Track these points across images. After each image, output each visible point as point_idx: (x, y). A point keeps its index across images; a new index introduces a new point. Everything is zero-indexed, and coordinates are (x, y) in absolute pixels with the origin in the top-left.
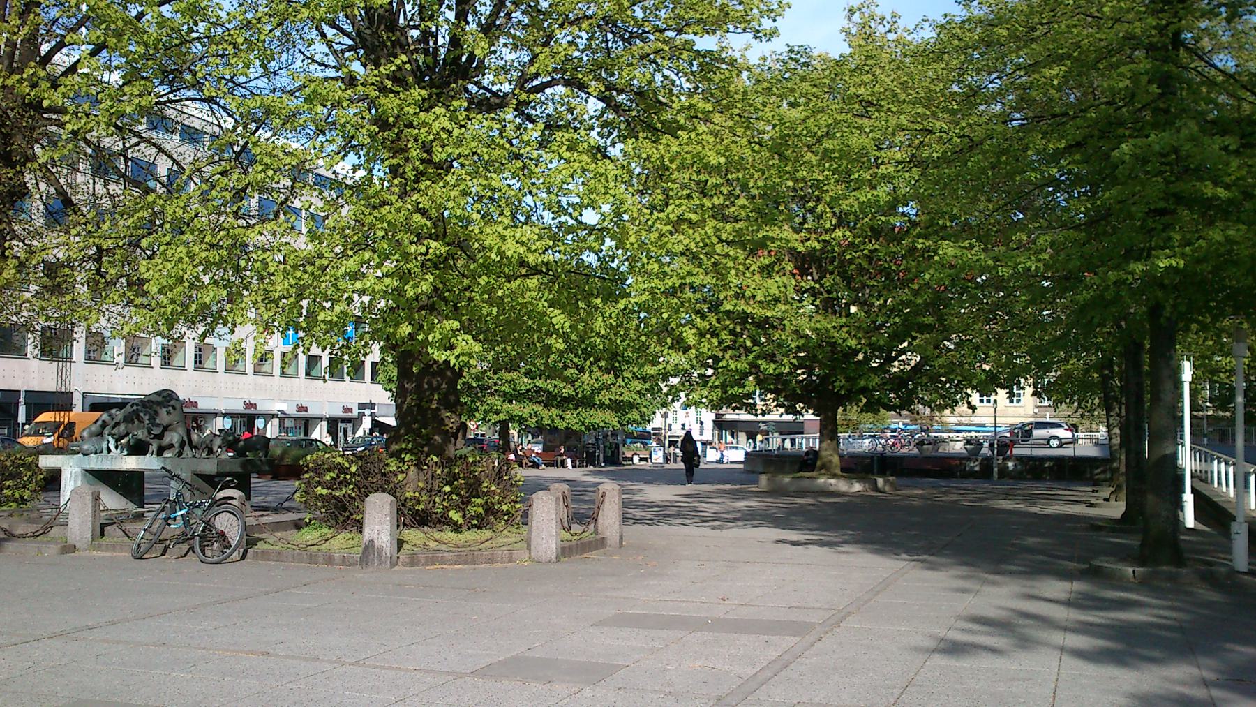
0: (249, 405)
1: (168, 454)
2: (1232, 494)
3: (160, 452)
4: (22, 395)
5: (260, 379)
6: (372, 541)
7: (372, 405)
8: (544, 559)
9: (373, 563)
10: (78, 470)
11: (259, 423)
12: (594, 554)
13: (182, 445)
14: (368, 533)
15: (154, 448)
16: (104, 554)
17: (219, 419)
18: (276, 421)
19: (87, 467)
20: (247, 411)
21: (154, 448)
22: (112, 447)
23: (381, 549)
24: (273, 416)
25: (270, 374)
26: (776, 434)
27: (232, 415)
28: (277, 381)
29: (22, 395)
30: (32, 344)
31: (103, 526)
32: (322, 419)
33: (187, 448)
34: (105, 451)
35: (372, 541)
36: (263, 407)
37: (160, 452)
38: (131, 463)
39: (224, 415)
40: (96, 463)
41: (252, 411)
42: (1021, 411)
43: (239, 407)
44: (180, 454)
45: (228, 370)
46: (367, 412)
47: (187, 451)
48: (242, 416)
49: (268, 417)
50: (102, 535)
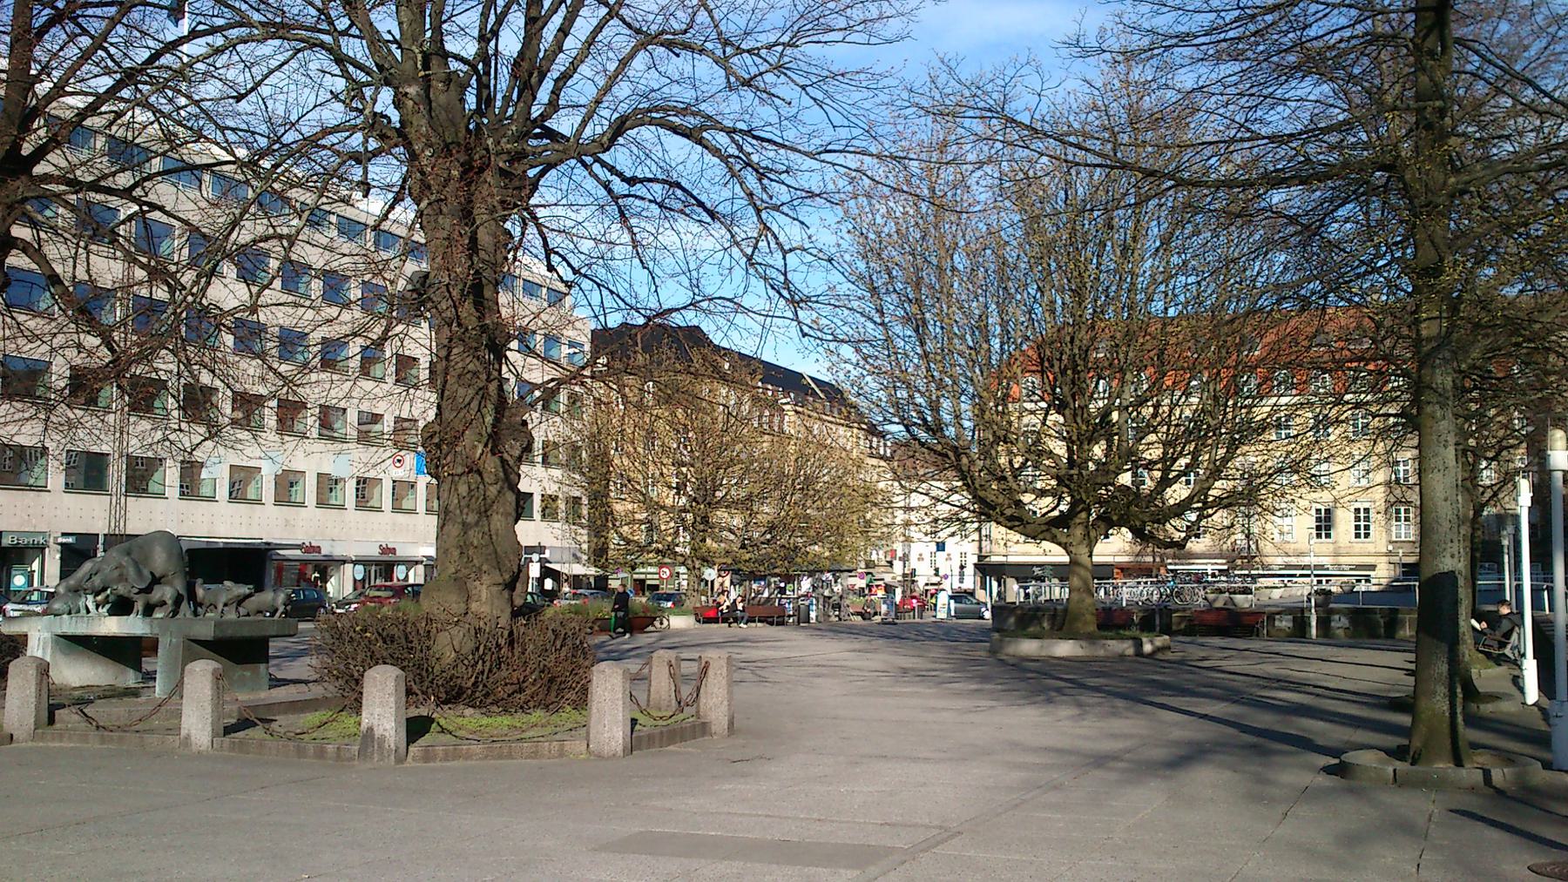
0: (386, 550)
1: (158, 614)
2: (1532, 694)
3: (149, 611)
4: (101, 540)
5: (400, 517)
6: (370, 729)
7: (540, 549)
8: (606, 750)
9: (372, 758)
10: (47, 635)
11: (400, 572)
12: (688, 748)
13: (178, 601)
14: (366, 719)
15: (139, 606)
16: (51, 745)
17: (349, 567)
18: (421, 568)
19: (59, 632)
20: (385, 558)
21: (139, 606)
22: (91, 606)
23: (382, 739)
24: (417, 563)
25: (413, 511)
26: (1056, 581)
27: (365, 562)
28: (352, 515)
29: (101, 540)
30: (56, 478)
31: (52, 710)
32: (417, 563)
33: (184, 605)
34: (83, 611)
35: (370, 729)
36: (402, 552)
37: (149, 611)
38: (112, 626)
39: (355, 563)
40: (70, 626)
41: (390, 557)
42: (1371, 548)
43: (373, 552)
44: (175, 612)
45: (322, 503)
46: (535, 557)
47: (185, 608)
48: (377, 563)
49: (411, 563)
50: (51, 720)
